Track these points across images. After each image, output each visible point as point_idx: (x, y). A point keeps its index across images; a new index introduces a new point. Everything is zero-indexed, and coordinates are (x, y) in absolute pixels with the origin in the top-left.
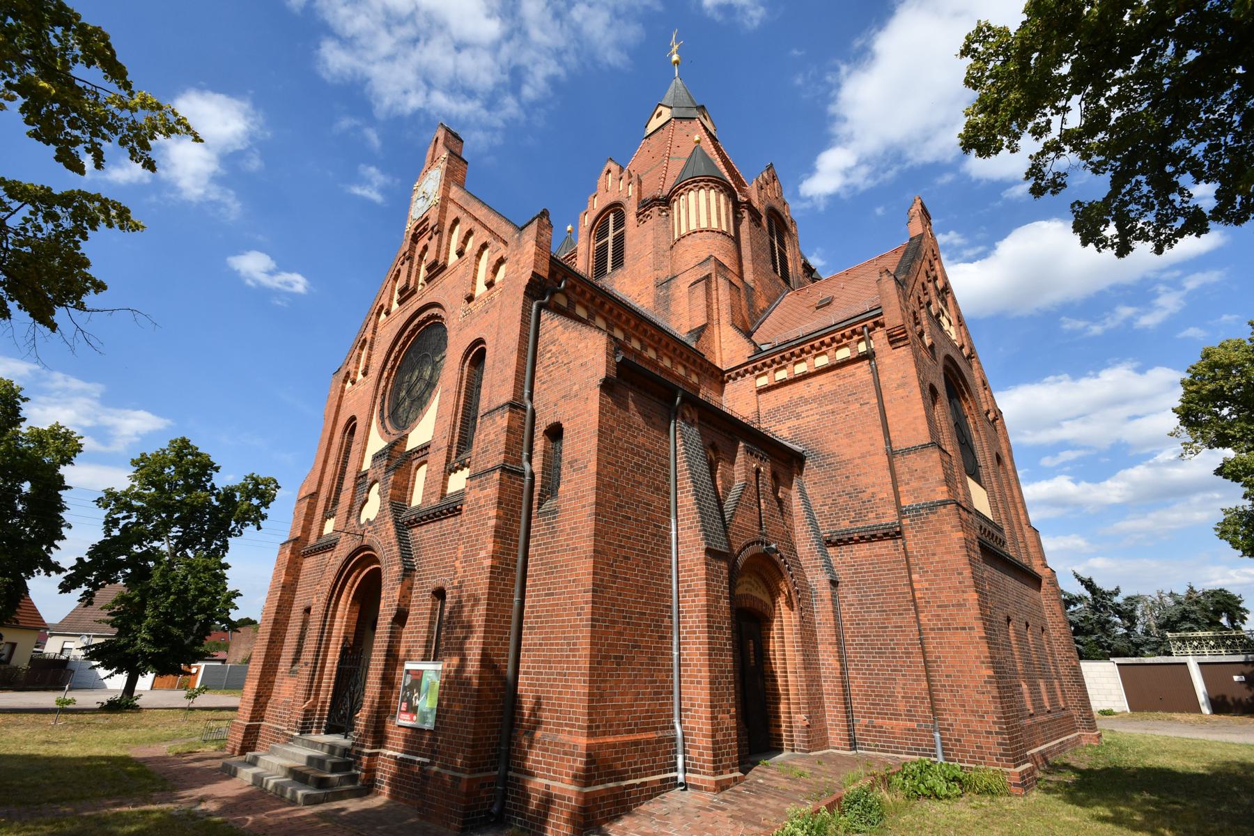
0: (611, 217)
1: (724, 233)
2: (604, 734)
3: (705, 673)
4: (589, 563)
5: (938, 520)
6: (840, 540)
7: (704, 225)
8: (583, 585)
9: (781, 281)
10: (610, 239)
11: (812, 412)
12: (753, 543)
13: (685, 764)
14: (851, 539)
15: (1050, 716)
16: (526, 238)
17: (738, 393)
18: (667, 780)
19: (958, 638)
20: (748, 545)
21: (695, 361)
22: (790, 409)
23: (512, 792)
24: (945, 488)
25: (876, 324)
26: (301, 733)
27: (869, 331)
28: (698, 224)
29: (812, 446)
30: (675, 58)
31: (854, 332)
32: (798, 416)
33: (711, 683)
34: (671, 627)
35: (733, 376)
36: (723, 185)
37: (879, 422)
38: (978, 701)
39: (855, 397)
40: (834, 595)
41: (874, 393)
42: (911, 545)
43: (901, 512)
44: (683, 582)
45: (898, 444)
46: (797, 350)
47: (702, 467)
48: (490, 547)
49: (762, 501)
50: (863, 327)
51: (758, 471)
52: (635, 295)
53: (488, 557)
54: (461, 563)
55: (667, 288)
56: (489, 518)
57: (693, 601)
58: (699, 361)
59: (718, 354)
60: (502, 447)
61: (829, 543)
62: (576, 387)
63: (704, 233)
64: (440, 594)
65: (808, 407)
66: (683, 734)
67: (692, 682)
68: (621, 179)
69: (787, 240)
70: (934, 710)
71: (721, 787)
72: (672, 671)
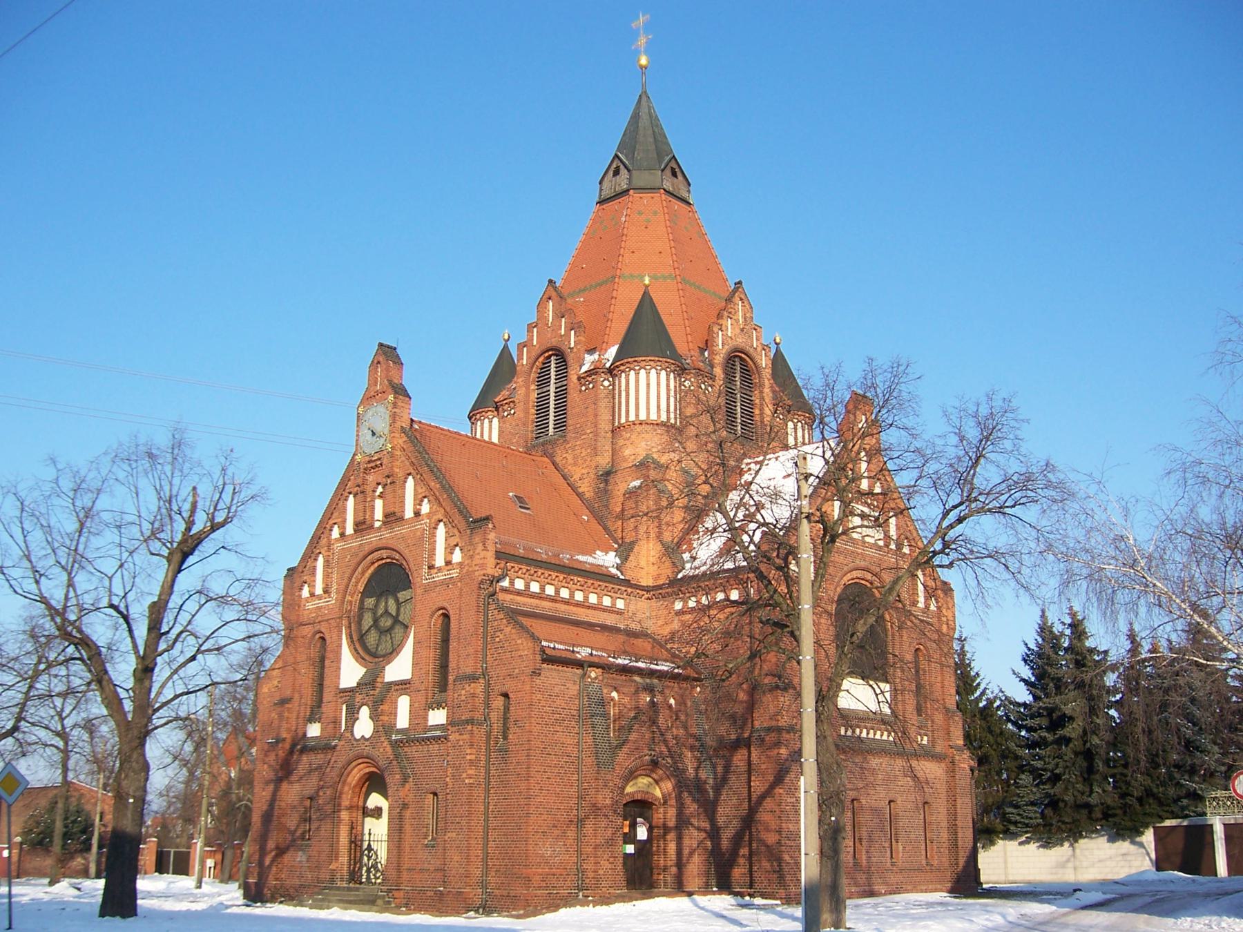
28: (637, 415)
52: (576, 477)
62: (517, 671)
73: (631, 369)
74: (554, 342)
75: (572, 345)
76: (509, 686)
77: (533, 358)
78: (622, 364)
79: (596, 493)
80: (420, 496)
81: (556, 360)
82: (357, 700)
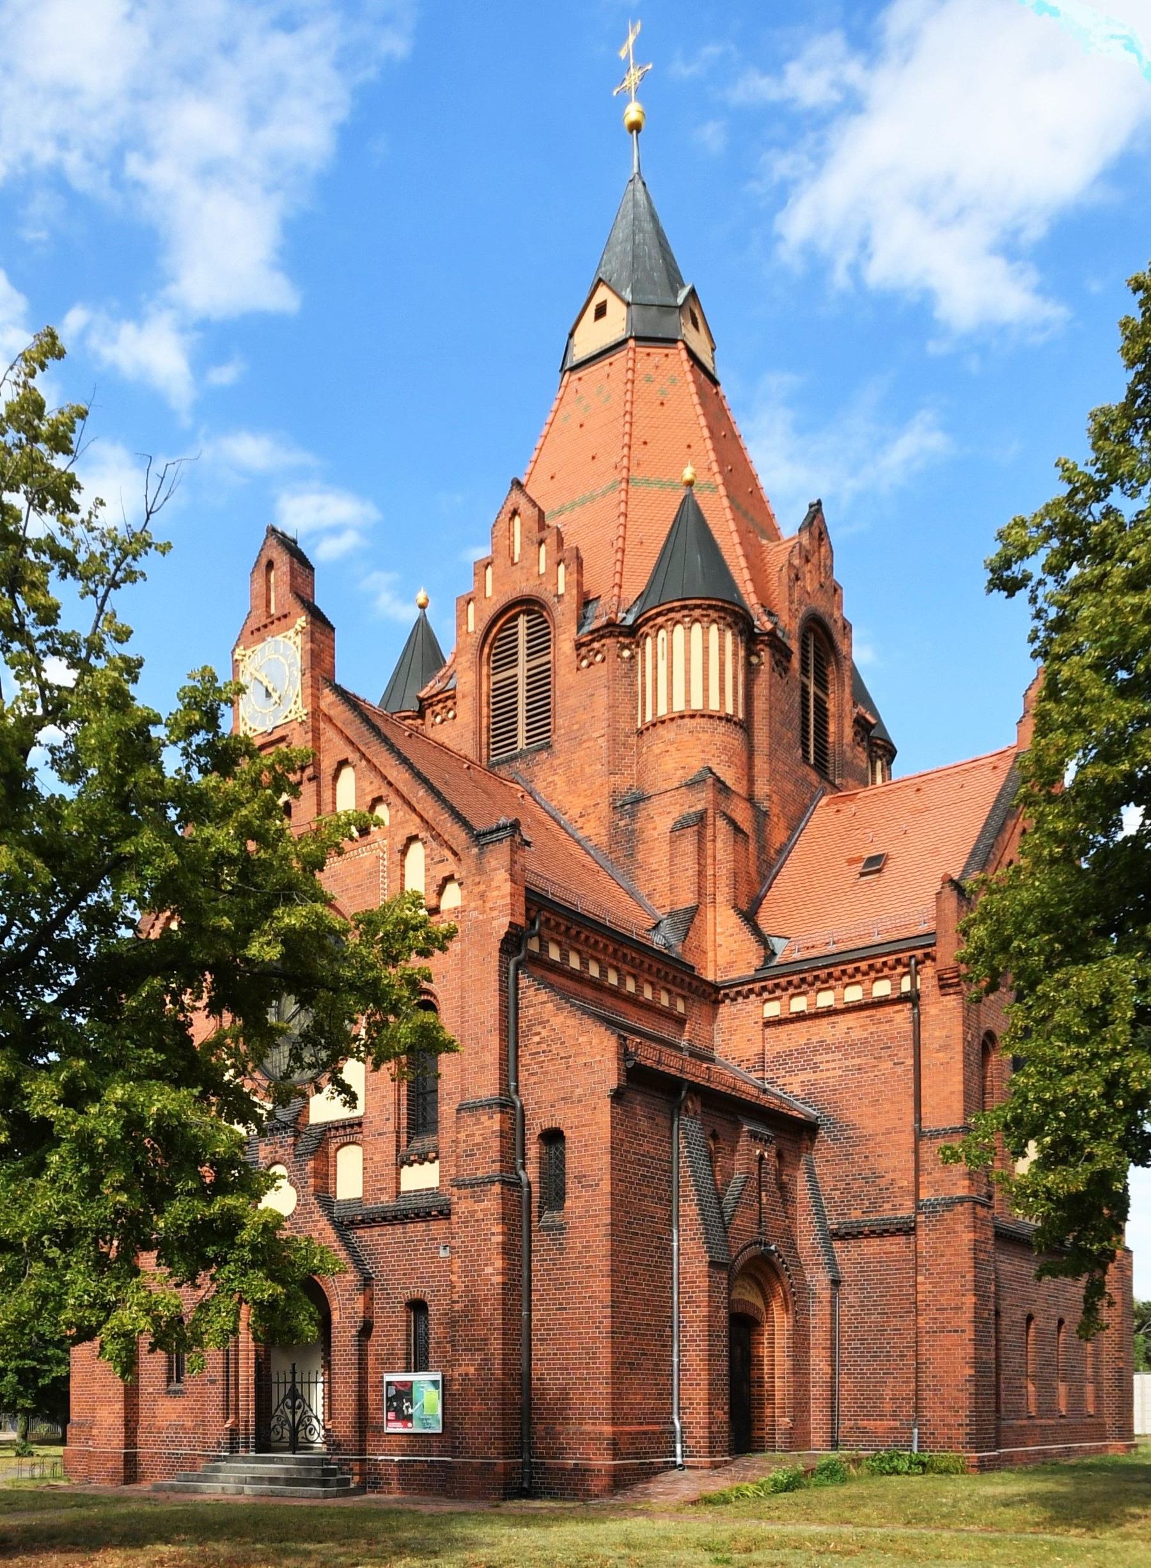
0: (522, 621)
1: (728, 719)
2: (622, 1424)
3: (704, 1375)
4: (607, 1282)
5: (952, 1219)
6: (848, 1234)
7: (697, 704)
8: (602, 1302)
9: (814, 777)
10: (521, 671)
11: (832, 1065)
12: (750, 1245)
13: (683, 1452)
14: (861, 1233)
15: (1062, 1421)
16: (494, 863)
17: (737, 1022)
18: (668, 1462)
19: (947, 1340)
20: (746, 1248)
21: (683, 980)
22: (805, 1057)
23: (537, 1473)
24: (967, 1183)
25: (927, 956)
26: (231, 1452)
27: (917, 963)
28: (688, 701)
29: (829, 1110)
30: (633, 112)
31: (898, 961)
32: (815, 1068)
33: (710, 1384)
34: (672, 1336)
35: (732, 995)
36: (734, 613)
37: (911, 1091)
38: (956, 1398)
39: (889, 1052)
40: (833, 1296)
41: (911, 1052)
42: (922, 1243)
43: (918, 1208)
44: (684, 1293)
45: (928, 1124)
46: (823, 974)
47: (703, 1164)
48: (499, 1264)
49: (763, 1194)
50: (911, 957)
51: (762, 1157)
52: (575, 812)
53: (498, 1274)
54: (460, 1277)
55: (633, 816)
56: (493, 1234)
57: (694, 1312)
58: (687, 980)
59: (710, 954)
60: (496, 1155)
61: (836, 1236)
62: (579, 1091)
63: (698, 720)
64: (418, 1307)
65: (830, 1057)
66: (682, 1428)
67: (691, 1385)
68: (541, 542)
69: (831, 671)
70: (917, 1409)
71: (715, 1466)
72: (672, 1375)
73: (678, 622)
74: (525, 588)
75: (561, 590)
76: (562, 1118)
77: (486, 619)
78: (659, 614)
79: (612, 837)
80: (369, 799)
81: (528, 621)
82: (262, 1154)
